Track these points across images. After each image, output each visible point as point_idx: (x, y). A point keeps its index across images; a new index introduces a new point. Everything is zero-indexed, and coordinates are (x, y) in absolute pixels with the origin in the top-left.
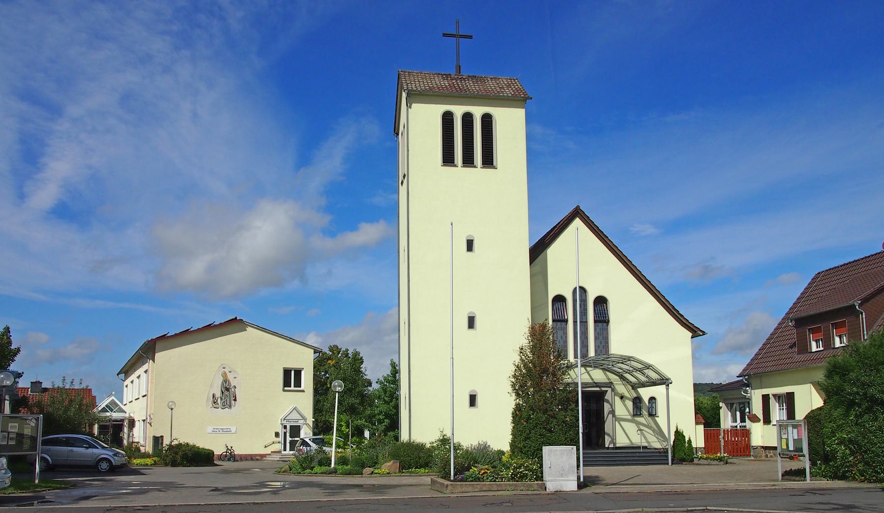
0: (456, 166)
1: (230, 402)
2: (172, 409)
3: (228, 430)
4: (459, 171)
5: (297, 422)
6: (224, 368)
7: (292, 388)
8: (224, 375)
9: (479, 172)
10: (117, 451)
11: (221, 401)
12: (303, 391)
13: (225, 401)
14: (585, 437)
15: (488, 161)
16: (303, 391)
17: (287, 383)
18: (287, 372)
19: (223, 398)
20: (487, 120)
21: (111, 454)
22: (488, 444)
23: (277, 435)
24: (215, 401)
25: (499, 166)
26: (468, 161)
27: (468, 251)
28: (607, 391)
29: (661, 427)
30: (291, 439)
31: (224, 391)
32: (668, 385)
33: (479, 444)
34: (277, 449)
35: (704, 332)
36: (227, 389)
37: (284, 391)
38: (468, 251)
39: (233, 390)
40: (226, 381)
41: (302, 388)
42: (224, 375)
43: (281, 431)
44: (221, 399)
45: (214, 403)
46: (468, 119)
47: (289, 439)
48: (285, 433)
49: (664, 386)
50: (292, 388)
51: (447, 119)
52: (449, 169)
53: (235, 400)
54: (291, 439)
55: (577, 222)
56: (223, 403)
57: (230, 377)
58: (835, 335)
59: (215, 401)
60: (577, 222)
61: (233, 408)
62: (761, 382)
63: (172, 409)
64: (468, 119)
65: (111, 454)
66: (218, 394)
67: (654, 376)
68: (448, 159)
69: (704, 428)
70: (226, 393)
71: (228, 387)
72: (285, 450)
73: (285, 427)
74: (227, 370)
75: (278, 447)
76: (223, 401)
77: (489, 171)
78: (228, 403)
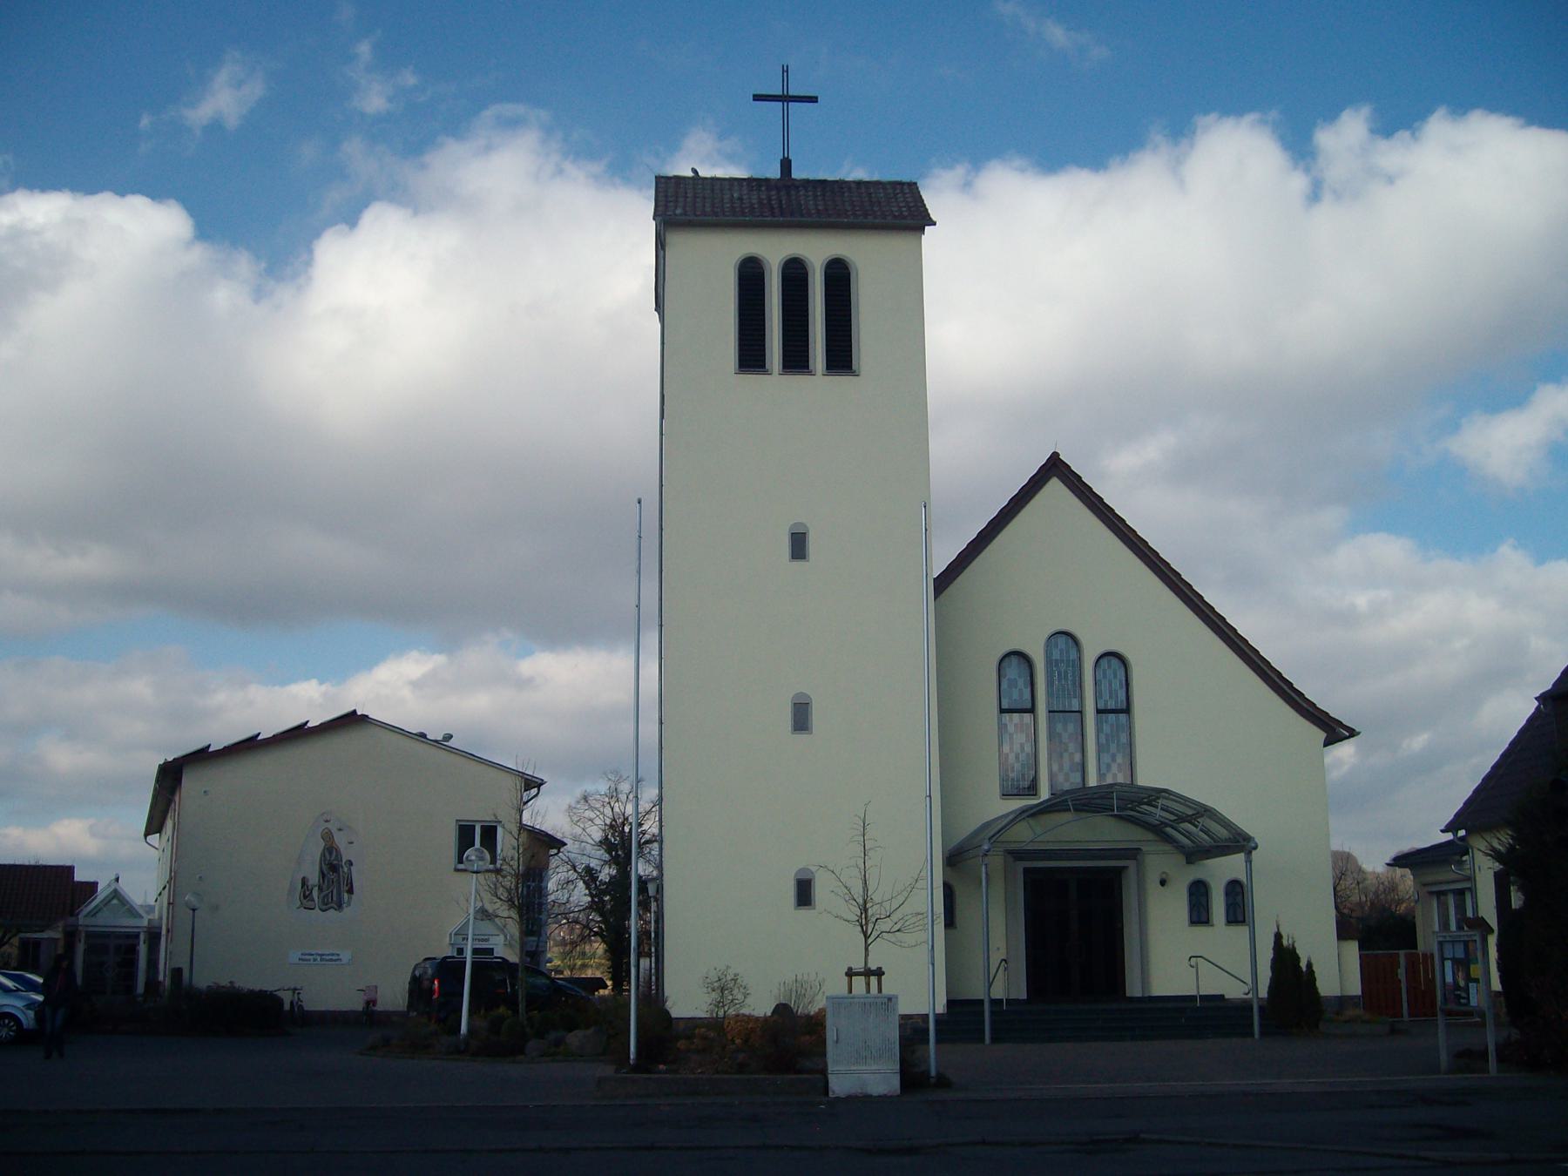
0: (810, 373)
1: (339, 894)
2: (194, 910)
3: (334, 958)
4: (775, 384)
5: (487, 940)
6: (327, 821)
8: (328, 836)
9: (818, 385)
10: (32, 999)
11: (319, 894)
13: (327, 895)
15: (841, 359)
19: (325, 887)
20: (839, 276)
21: (20, 1004)
22: (731, 972)
24: (307, 893)
25: (863, 372)
26: (796, 360)
27: (804, 558)
28: (1125, 868)
31: (326, 872)
32: (1250, 852)
35: (1354, 730)
36: (334, 868)
37: (457, 870)
38: (804, 558)
39: (346, 870)
40: (330, 849)
42: (328, 836)
44: (321, 889)
45: (305, 897)
46: (795, 273)
49: (1241, 856)
51: (750, 276)
52: (752, 380)
53: (351, 891)
55: (1055, 486)
56: (324, 897)
57: (340, 840)
59: (307, 893)
60: (1055, 486)
61: (346, 910)
63: (194, 910)
64: (795, 273)
65: (20, 1004)
66: (314, 879)
67: (1223, 833)
68: (751, 357)
69: (1361, 948)
70: (332, 876)
71: (335, 862)
74: (333, 827)
76: (324, 893)
77: (841, 381)
78: (335, 899)
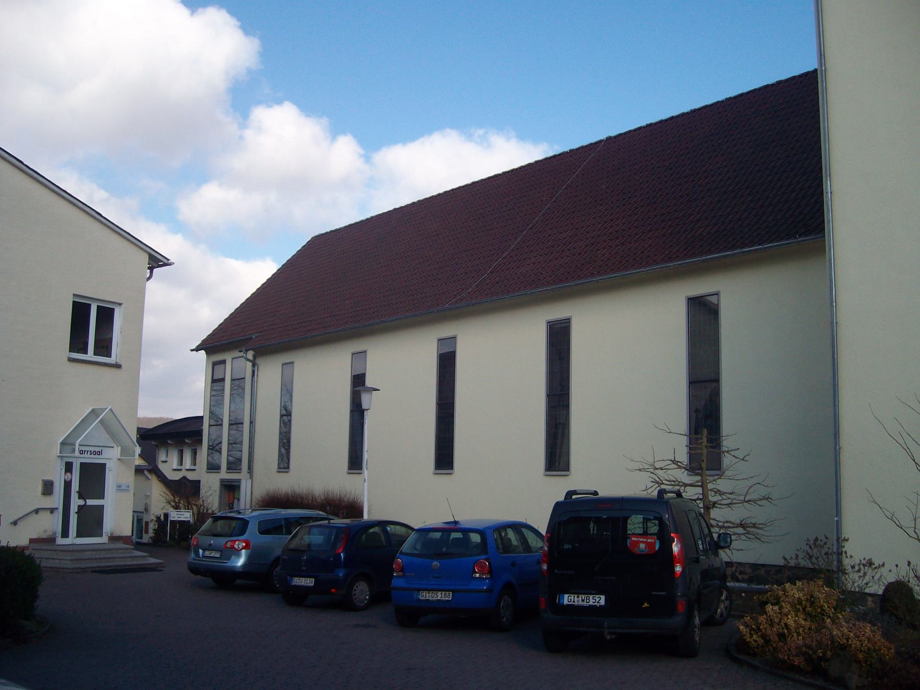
7: (90, 355)
12: (118, 366)
14: (296, 256)
16: (118, 366)
17: (78, 342)
18: (80, 311)
23: (48, 488)
29: (548, 521)
30: (82, 502)
33: (346, 495)
34: (45, 531)
37: (71, 360)
41: (112, 360)
43: (58, 479)
47: (76, 502)
48: (68, 485)
50: (90, 355)
54: (82, 502)
58: (144, 532)
62: (167, 453)
72: (65, 534)
73: (69, 467)
75: (50, 524)
